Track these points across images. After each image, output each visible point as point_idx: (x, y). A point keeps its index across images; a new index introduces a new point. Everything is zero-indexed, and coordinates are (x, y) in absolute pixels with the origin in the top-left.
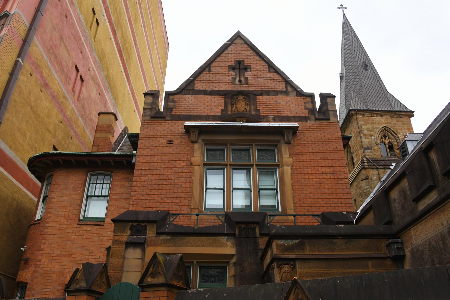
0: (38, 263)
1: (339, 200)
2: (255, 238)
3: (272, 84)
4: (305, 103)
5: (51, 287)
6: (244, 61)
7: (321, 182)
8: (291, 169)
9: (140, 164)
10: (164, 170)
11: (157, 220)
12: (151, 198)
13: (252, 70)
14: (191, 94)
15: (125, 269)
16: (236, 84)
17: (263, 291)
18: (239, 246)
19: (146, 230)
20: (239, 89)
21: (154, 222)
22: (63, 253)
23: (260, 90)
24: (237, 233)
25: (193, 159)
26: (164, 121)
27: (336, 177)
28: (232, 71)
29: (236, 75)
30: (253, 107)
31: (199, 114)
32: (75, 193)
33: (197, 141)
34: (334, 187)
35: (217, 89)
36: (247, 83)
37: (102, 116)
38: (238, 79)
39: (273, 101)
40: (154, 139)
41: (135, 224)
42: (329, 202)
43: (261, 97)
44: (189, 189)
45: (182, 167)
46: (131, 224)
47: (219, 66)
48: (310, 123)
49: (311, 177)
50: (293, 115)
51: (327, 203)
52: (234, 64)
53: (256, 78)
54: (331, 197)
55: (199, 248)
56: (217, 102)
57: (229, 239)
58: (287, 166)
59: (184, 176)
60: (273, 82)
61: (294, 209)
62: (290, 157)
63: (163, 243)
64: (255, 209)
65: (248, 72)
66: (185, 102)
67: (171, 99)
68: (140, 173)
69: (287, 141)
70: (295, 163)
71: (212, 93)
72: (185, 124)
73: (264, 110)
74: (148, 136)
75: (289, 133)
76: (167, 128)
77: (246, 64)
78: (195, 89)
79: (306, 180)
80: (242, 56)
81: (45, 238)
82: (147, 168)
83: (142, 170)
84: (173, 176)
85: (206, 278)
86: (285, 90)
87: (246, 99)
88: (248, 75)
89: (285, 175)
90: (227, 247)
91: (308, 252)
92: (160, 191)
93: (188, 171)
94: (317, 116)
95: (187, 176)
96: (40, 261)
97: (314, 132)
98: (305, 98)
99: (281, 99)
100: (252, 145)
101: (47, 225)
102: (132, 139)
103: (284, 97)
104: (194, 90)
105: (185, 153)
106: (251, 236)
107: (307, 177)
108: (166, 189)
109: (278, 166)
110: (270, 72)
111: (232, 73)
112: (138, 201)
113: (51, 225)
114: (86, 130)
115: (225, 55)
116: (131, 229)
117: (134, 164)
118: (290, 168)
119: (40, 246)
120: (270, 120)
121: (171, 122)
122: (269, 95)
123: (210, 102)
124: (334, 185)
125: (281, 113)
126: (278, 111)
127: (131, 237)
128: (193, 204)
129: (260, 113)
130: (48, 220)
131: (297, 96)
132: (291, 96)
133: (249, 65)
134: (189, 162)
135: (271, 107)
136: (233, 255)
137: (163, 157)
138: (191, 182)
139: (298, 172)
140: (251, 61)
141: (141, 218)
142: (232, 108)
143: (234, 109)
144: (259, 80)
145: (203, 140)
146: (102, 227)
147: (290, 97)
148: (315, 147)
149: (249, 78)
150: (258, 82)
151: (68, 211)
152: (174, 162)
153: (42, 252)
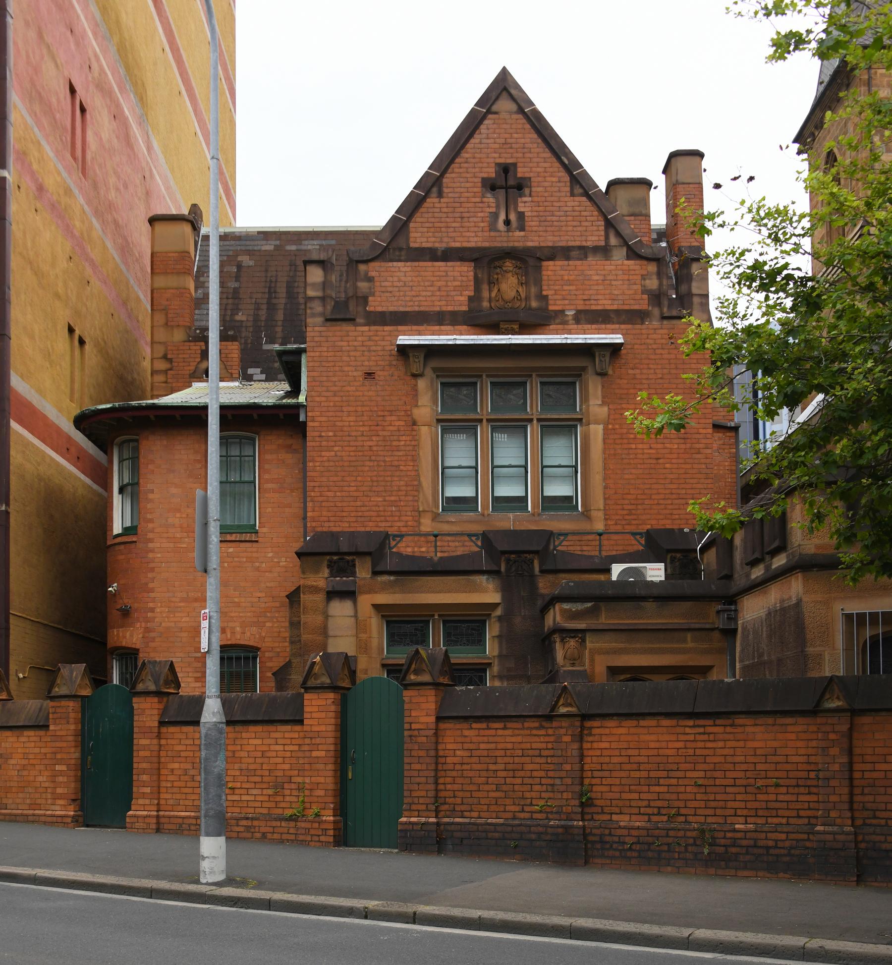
0: (150, 615)
1: (689, 491)
2: (532, 576)
3: (575, 229)
4: (643, 277)
5: (181, 655)
6: (515, 165)
7: (660, 456)
8: (604, 430)
9: (316, 424)
10: (363, 435)
11: (371, 550)
12: (344, 494)
13: (533, 189)
14: (403, 258)
15: (331, 633)
16: (499, 231)
17: (535, 692)
18: (506, 589)
19: (355, 567)
20: (505, 245)
21: (369, 554)
22: (191, 594)
23: (550, 244)
24: (503, 569)
25: (416, 412)
26: (353, 328)
27: (688, 446)
28: (489, 195)
29: (498, 207)
30: (533, 290)
31: (422, 309)
32: (191, 480)
33: (423, 372)
34: (683, 466)
35: (458, 245)
36: (522, 228)
37: (160, 227)
38: (502, 217)
39: (576, 273)
40: (337, 369)
41: (335, 558)
42: (670, 496)
43: (551, 263)
44: (413, 473)
45: (395, 428)
46: (328, 557)
47: (461, 180)
48: (651, 326)
49: (640, 446)
50: (615, 307)
51: (667, 497)
52: (494, 175)
53: (541, 214)
54: (675, 486)
55: (441, 595)
56: (460, 278)
57: (491, 579)
58: (597, 423)
59: (403, 448)
60: (578, 224)
61: (605, 509)
62: (604, 403)
63: (384, 588)
64: (533, 507)
65: (525, 196)
66: (391, 279)
67: (362, 273)
68: (318, 444)
69: (599, 370)
70: (612, 417)
71: (449, 255)
72: (398, 343)
73: (556, 297)
74: (324, 364)
75: (604, 356)
76: (360, 343)
77: (521, 172)
78: (412, 245)
79: (631, 452)
80: (511, 151)
81: (152, 570)
82: (331, 434)
83: (320, 436)
84: (381, 448)
85: (453, 638)
86: (603, 243)
87: (520, 268)
88: (524, 205)
89: (592, 442)
90: (486, 592)
91: (604, 620)
92: (359, 479)
93: (408, 438)
94: (665, 309)
95: (408, 448)
96: (152, 610)
97: (655, 346)
98: (645, 262)
99: (594, 267)
100: (531, 376)
101: (150, 545)
102: (285, 358)
103: (599, 262)
104: (409, 248)
105: (400, 400)
106: (526, 574)
107: (633, 446)
108: (370, 474)
109: (580, 420)
110: (572, 194)
111: (490, 199)
112: (321, 499)
113: (158, 545)
114: (101, 233)
115: (474, 148)
116: (329, 566)
117: (304, 424)
118: (601, 427)
119: (147, 584)
120: (568, 321)
121: (366, 328)
122: (568, 258)
123: (444, 279)
124: (682, 461)
125: (592, 302)
126: (585, 297)
127: (332, 580)
128: (422, 503)
129: (547, 304)
130: (150, 535)
131: (628, 258)
132: (615, 258)
133: (527, 175)
134: (410, 419)
135: (571, 288)
136: (497, 605)
137: (359, 409)
138: (415, 459)
139: (616, 436)
140: (531, 165)
141: (344, 548)
142: (490, 291)
143: (493, 295)
144: (549, 218)
145: (435, 370)
146: (255, 545)
147: (613, 262)
148: (653, 381)
149: (526, 214)
151: (184, 516)
152: (381, 418)
153: (152, 595)
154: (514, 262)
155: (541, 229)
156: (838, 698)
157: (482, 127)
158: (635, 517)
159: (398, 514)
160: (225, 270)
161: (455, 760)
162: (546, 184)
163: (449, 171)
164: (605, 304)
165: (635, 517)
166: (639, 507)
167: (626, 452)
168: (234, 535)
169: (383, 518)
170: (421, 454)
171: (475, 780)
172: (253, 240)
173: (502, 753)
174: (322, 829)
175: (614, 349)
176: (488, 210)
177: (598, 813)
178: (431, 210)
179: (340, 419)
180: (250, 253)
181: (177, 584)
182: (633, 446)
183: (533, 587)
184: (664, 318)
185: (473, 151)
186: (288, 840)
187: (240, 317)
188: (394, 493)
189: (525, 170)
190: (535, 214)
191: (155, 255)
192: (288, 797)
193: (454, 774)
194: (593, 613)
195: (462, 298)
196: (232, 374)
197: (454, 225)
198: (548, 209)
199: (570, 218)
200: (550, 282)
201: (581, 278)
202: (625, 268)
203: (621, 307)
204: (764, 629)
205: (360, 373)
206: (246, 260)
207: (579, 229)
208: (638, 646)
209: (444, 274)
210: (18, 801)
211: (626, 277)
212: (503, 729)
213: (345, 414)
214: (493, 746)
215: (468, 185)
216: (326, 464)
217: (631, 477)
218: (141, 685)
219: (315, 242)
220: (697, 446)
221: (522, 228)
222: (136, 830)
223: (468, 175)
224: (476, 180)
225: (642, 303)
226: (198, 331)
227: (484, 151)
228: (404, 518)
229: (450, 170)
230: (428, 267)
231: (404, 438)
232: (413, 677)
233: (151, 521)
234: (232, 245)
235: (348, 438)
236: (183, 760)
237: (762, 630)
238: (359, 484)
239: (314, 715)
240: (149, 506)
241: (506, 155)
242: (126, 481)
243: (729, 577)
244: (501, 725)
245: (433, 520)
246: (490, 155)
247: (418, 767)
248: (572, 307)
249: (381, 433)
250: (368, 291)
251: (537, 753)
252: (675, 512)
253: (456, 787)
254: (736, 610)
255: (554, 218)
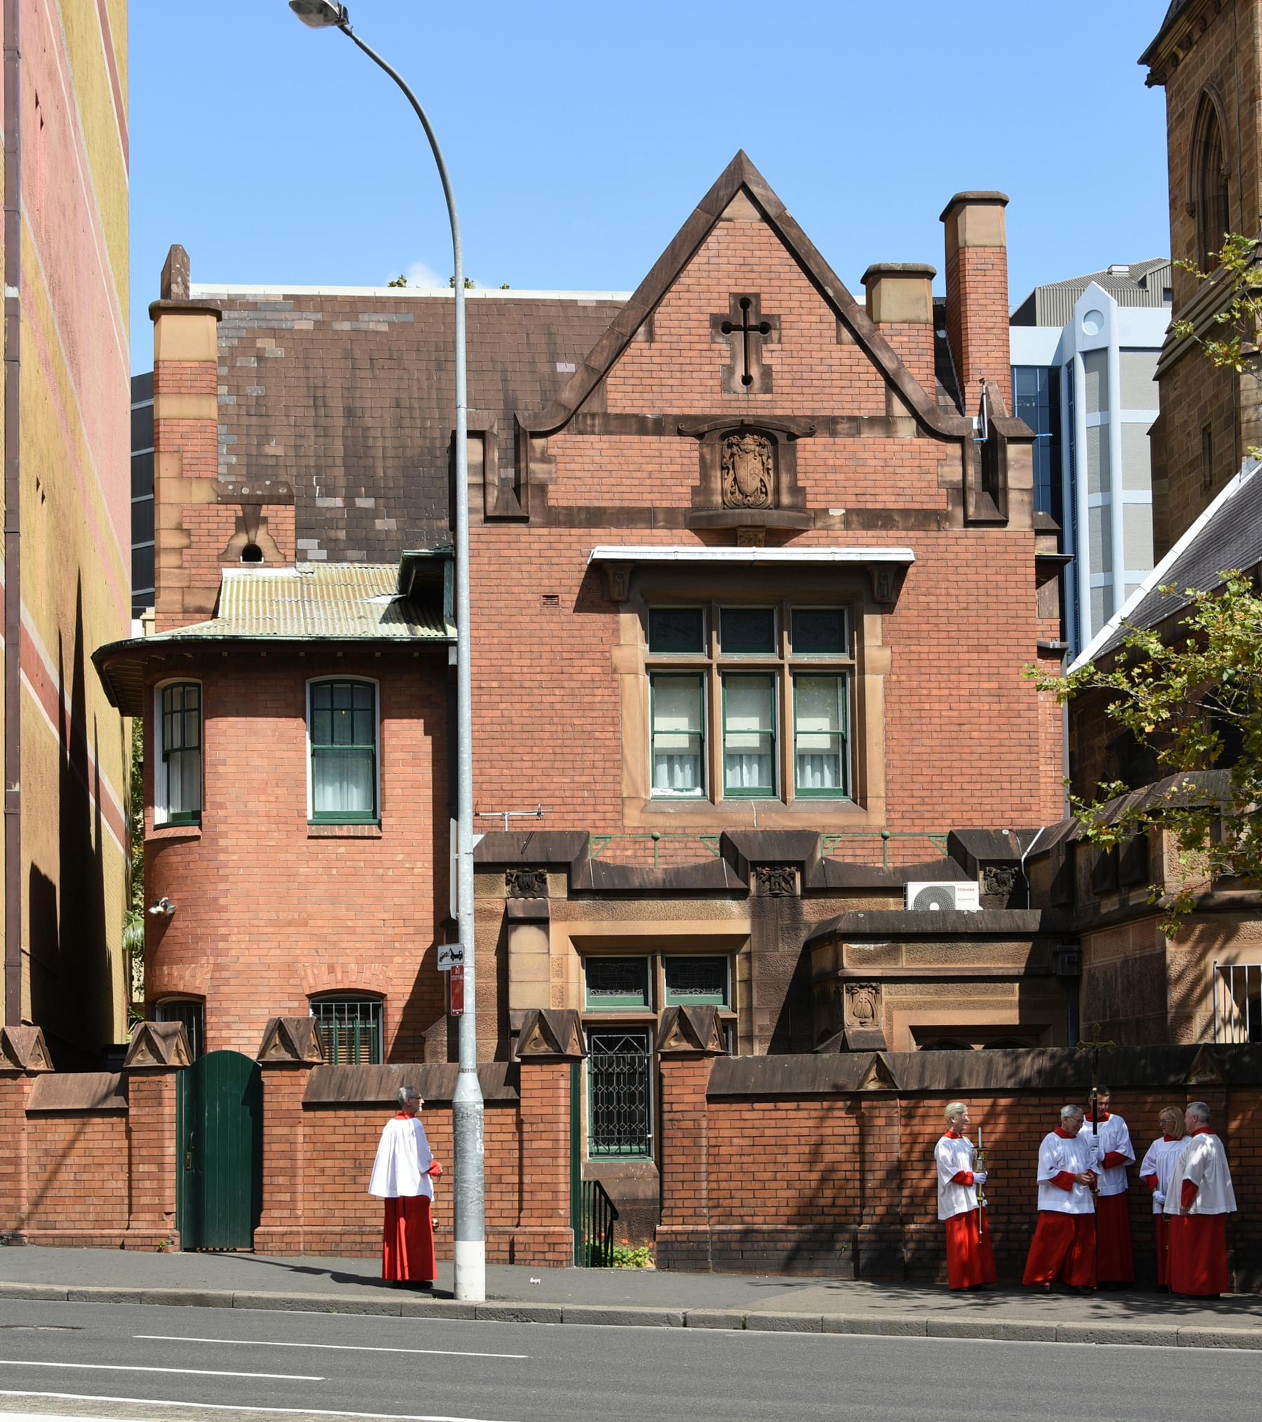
0: (221, 945)
1: (1005, 771)
6: (757, 296)
7: (963, 721)
11: (569, 860)
12: (513, 772)
13: (784, 333)
19: (546, 883)
22: (282, 915)
23: (809, 413)
26: (526, 530)
27: (1004, 706)
29: (733, 357)
31: (625, 504)
34: (996, 735)
36: (767, 389)
38: (740, 371)
39: (845, 455)
43: (809, 440)
44: (613, 743)
45: (588, 677)
49: (936, 706)
50: (901, 506)
52: (727, 311)
53: (795, 368)
54: (986, 764)
56: (679, 460)
58: (875, 672)
60: (848, 384)
62: (885, 644)
65: (772, 343)
67: (538, 450)
70: (896, 664)
71: (659, 427)
77: (767, 307)
81: (225, 879)
82: (495, 684)
84: (568, 706)
88: (772, 355)
90: (730, 918)
92: (536, 750)
93: (606, 692)
95: (605, 707)
96: (225, 938)
97: (956, 563)
104: (606, 415)
108: (550, 743)
110: (839, 342)
111: (722, 345)
113: (234, 842)
118: (881, 677)
119: (216, 899)
121: (545, 531)
122: (833, 434)
124: (995, 728)
129: (805, 501)
130: (222, 828)
133: (775, 312)
135: (838, 477)
137: (535, 648)
140: (780, 297)
144: (806, 375)
148: (955, 613)
150: (803, 383)
153: (224, 916)
154: (756, 437)
155: (795, 390)
156: (1212, 1071)
157: (710, 239)
158: (929, 808)
159: (592, 801)
160: (238, 364)
161: (731, 1150)
162: (803, 325)
163: (663, 304)
164: (886, 501)
165: (929, 808)
166: (935, 793)
167: (916, 714)
168: (345, 827)
169: (570, 808)
170: (624, 715)
171: (759, 1176)
172: (277, 310)
173: (795, 1140)
174: (549, 1244)
175: (901, 568)
176: (718, 361)
177: (920, 1214)
178: (637, 360)
179: (508, 662)
180: (274, 333)
181: (262, 900)
182: (927, 706)
183: (796, 912)
184: (968, 523)
185: (697, 274)
186: (498, 1260)
187: (273, 449)
188: (587, 771)
189: (772, 303)
190: (786, 368)
191: (161, 364)
192: (496, 1203)
193: (731, 1168)
194: (893, 955)
195: (683, 490)
196: (285, 556)
197: (671, 382)
198: (804, 361)
199: (837, 376)
200: (810, 469)
201: (851, 463)
202: (913, 448)
203: (909, 506)
204: (1119, 981)
205: (536, 597)
206: (268, 345)
207: (850, 391)
208: (951, 998)
209: (657, 454)
210: (74, 1217)
211: (916, 463)
212: (795, 1110)
213: (516, 655)
214: (782, 1132)
215: (691, 324)
216: (488, 728)
217: (923, 750)
218: (273, 1052)
219: (381, 317)
220: (1016, 706)
221: (767, 389)
222: (270, 1253)
223: (691, 310)
224: (702, 317)
225: (940, 501)
226: (231, 487)
227: (713, 274)
228: (601, 808)
229: (664, 302)
230: (636, 444)
231: (600, 691)
232: (673, 1043)
233: (222, 806)
234: (244, 319)
235: (519, 691)
236: (339, 1155)
237: (1116, 981)
238: (535, 757)
239: (536, 1093)
240: (219, 784)
241: (744, 282)
242: (168, 747)
243: (1071, 904)
244: (793, 1105)
245: (643, 811)
246: (722, 281)
247: (682, 1159)
248: (839, 505)
249: (566, 684)
250: (546, 476)
251: (841, 1139)
252: (985, 801)
253: (732, 1185)
254: (1080, 952)
255: (814, 376)
